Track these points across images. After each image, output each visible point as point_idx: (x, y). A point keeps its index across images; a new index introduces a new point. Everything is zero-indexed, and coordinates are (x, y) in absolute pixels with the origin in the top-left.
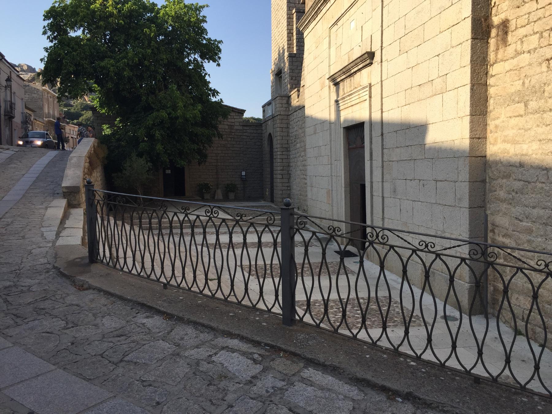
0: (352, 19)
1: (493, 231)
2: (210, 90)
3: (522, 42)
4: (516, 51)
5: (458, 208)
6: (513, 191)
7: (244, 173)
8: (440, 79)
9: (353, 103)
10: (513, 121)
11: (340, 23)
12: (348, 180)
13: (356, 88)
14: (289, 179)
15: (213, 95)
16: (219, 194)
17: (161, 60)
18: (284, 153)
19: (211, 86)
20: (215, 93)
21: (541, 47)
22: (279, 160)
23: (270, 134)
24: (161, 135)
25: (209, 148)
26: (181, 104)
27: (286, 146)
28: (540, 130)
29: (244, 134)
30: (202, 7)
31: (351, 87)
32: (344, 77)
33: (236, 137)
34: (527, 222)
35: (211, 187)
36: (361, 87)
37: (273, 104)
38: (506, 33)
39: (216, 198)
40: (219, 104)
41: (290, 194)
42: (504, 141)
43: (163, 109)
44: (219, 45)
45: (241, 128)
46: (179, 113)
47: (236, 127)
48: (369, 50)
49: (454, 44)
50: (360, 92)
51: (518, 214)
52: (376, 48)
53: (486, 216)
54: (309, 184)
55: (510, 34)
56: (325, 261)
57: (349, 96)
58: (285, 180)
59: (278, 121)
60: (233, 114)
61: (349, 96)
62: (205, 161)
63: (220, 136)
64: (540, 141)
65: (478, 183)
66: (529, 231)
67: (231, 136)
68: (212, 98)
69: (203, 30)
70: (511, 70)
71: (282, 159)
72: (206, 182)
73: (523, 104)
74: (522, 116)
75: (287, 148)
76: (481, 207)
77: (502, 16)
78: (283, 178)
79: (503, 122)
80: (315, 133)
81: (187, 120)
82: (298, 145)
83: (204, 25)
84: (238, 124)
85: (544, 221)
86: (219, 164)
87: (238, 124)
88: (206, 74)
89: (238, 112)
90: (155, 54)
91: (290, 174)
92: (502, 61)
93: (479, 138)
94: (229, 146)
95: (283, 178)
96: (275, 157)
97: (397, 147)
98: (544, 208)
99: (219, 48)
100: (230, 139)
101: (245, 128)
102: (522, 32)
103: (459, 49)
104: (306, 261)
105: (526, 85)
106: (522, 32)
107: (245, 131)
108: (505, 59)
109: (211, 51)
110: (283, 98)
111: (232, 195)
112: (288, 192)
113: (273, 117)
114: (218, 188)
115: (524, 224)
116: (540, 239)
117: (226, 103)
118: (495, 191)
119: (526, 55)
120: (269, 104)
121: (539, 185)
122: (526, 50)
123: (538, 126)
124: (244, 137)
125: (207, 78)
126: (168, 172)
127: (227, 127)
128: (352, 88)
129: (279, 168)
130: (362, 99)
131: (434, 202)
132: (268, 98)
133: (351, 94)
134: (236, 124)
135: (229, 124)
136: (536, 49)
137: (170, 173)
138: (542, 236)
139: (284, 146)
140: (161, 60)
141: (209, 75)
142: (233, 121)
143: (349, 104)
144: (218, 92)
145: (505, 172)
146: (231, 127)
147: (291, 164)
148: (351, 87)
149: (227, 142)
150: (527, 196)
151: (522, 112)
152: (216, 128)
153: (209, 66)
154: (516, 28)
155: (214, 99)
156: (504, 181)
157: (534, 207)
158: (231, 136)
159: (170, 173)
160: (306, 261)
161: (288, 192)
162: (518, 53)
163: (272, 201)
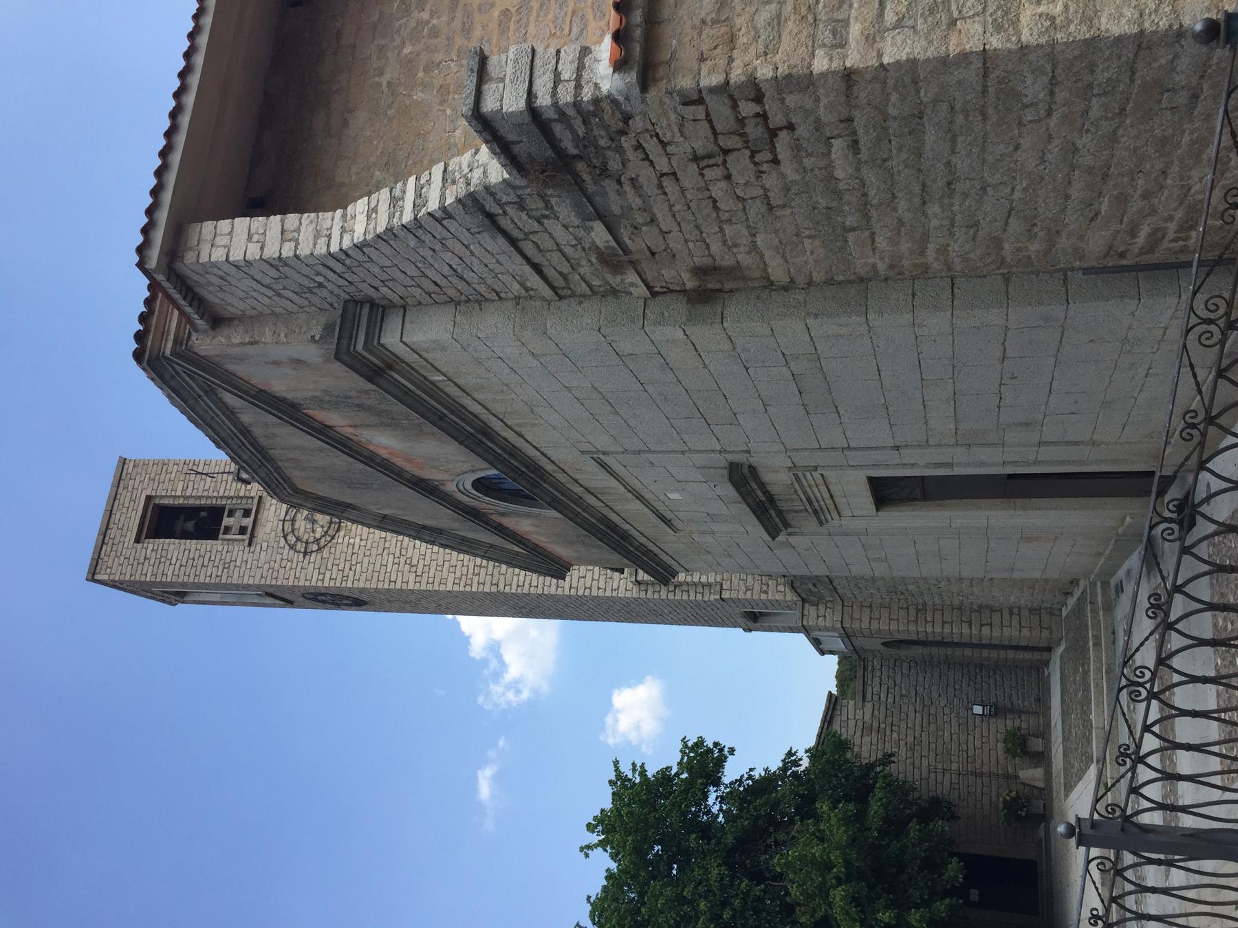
0: (662, 497)
1: (1122, 255)
2: (784, 769)
3: (735, 246)
4: (749, 253)
5: (1069, 321)
6: (1029, 231)
7: (978, 710)
8: (792, 364)
9: (826, 495)
10: (882, 243)
11: (668, 515)
12: (999, 501)
13: (796, 491)
14: (992, 610)
15: (796, 763)
16: (1031, 774)
17: (722, 879)
18: (929, 619)
19: (773, 769)
20: (790, 759)
21: (747, 219)
22: (947, 630)
23: (883, 644)
24: (886, 907)
25: (917, 795)
26: (817, 851)
27: (912, 612)
28: (902, 204)
29: (883, 699)
30: (619, 775)
31: (792, 500)
32: (772, 512)
33: (889, 720)
34: (1101, 203)
35: (1013, 794)
36: (796, 484)
37: (817, 634)
38: (716, 269)
39: (1041, 785)
40: (814, 753)
41: (1030, 610)
42: (922, 253)
43: (827, 895)
44: (690, 744)
45: (869, 706)
46: (835, 856)
47: (868, 717)
48: (726, 472)
49: (728, 346)
50: (805, 483)
51: (1081, 218)
52: (722, 460)
53: (1087, 271)
54: (1005, 575)
55: (719, 262)
56: (1214, 711)
57: (810, 503)
58: (996, 618)
59: (856, 625)
60: (836, 727)
61: (810, 503)
62: (949, 803)
63: (887, 759)
64: (924, 203)
65: (1011, 289)
66: (1122, 200)
67: (888, 732)
68: (802, 768)
69: (663, 777)
70: (783, 256)
71: (943, 623)
72: (1001, 805)
73: (850, 235)
74: (873, 235)
75: (918, 611)
76: (1066, 279)
77: (685, 276)
78: (990, 625)
79: (882, 259)
80: (886, 560)
81: (853, 841)
82: (911, 588)
83: (651, 773)
84: (859, 712)
85: (1099, 179)
86: (954, 766)
87: (859, 712)
88: (750, 777)
89: (834, 709)
90: (709, 891)
91: (980, 607)
92: (765, 270)
93: (913, 295)
94: (910, 739)
95: (990, 625)
96: (940, 639)
97: (926, 423)
98: (1070, 183)
99: (696, 744)
100: (895, 735)
101: (869, 696)
102: (716, 247)
103: (739, 341)
104: (1215, 749)
105: (813, 232)
106: (716, 247)
107: (875, 698)
108: (762, 266)
109: (704, 761)
110: (806, 612)
111: (1036, 744)
112: (1025, 612)
113: (847, 635)
114: (1016, 777)
115: (1104, 208)
116: (1140, 182)
117: (812, 742)
118: (1029, 257)
119: (759, 239)
120: (816, 643)
121: (1017, 195)
122: (750, 239)
123: (895, 209)
124: (890, 700)
125: (756, 775)
126: (974, 895)
127: (866, 739)
128: (795, 497)
129: (966, 630)
130: (820, 481)
131: (1053, 360)
132: (800, 641)
133: (809, 499)
134: (859, 716)
135: (859, 733)
136: (749, 227)
137: (976, 892)
138: (1133, 179)
139: (912, 618)
140: (722, 879)
141: (751, 770)
142: (852, 723)
143: (829, 502)
144: (790, 754)
145: (988, 247)
146: (866, 729)
147: (956, 602)
148: (792, 500)
149: (902, 743)
150: (1041, 210)
151: (867, 233)
152: (870, 767)
153: (732, 771)
154: (710, 255)
155: (805, 763)
156: (1006, 245)
157: (1067, 197)
158: (888, 732)
159: (976, 892)
160: (1215, 749)
161: (1025, 612)
162: (754, 248)
163: (1049, 649)
